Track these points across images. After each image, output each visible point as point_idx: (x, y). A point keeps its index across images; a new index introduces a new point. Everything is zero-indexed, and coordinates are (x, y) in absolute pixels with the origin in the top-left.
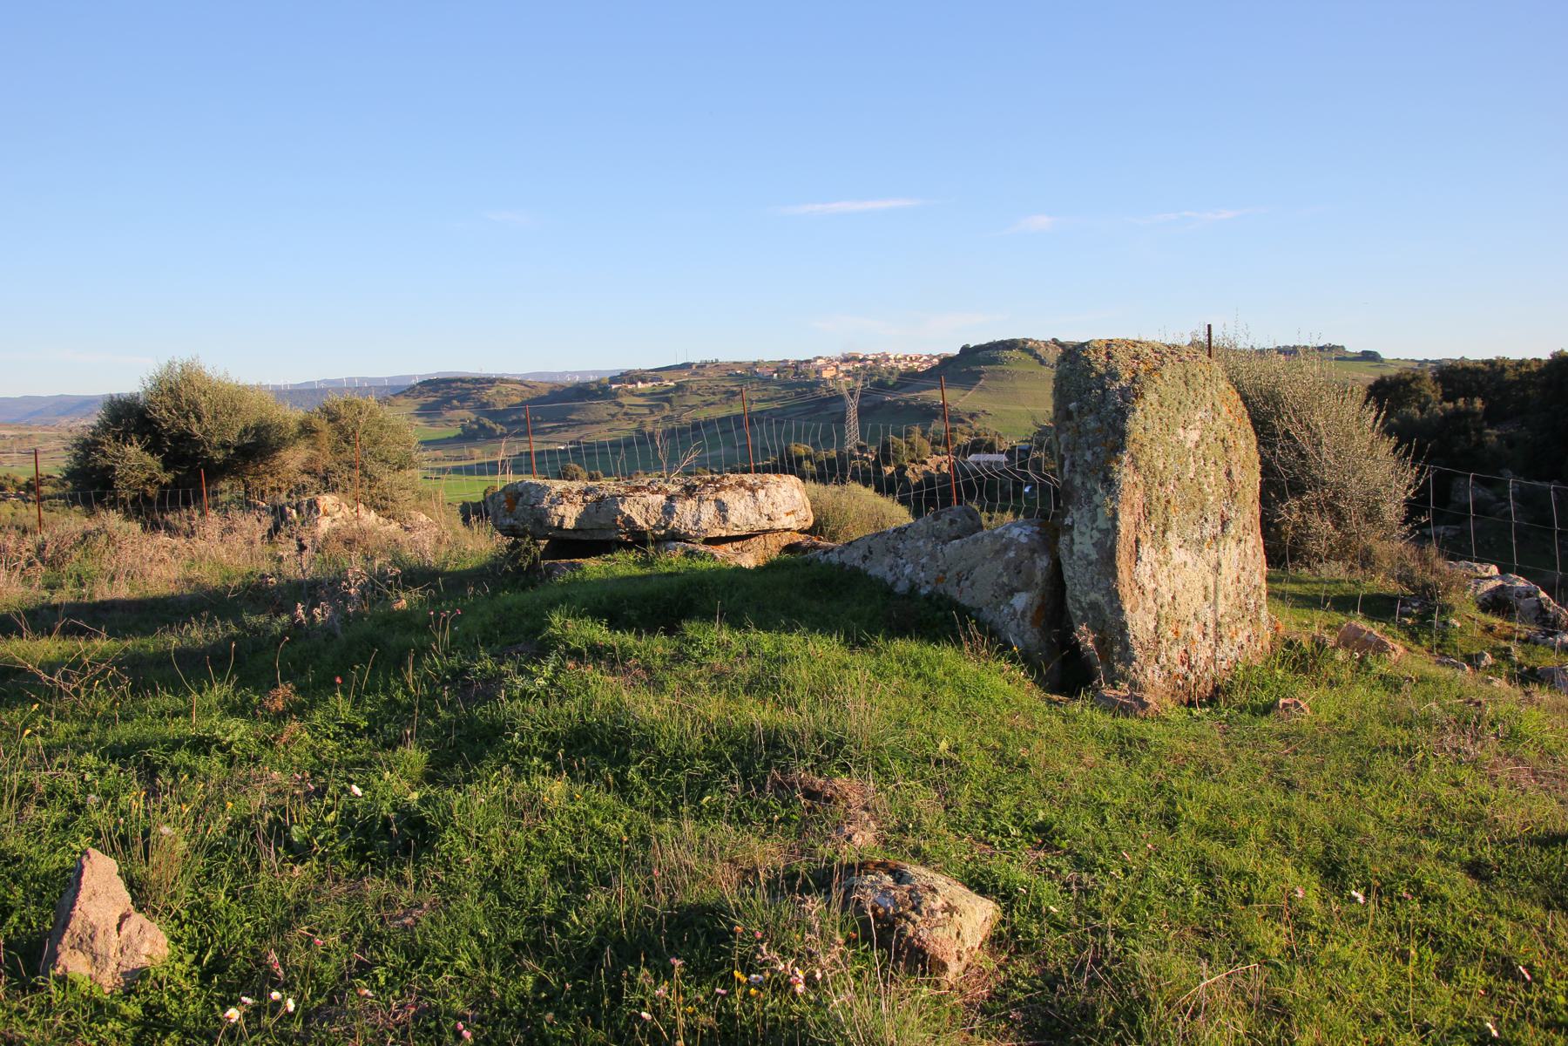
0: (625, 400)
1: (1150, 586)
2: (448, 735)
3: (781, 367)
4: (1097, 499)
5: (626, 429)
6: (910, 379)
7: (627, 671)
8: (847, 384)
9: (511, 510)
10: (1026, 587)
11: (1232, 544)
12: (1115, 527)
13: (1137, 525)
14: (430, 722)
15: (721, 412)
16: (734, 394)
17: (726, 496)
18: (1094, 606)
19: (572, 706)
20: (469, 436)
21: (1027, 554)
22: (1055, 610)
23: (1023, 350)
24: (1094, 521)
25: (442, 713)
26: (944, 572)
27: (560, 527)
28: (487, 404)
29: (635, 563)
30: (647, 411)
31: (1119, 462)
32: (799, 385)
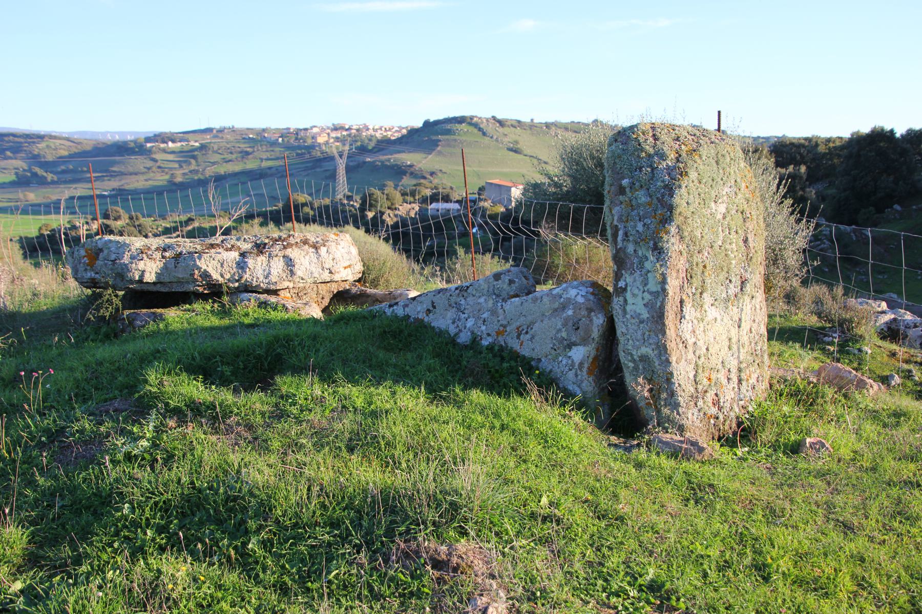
0: (158, 156)
1: (691, 341)
2: (50, 506)
3: (285, 133)
4: (648, 265)
5: (161, 179)
6: (385, 145)
7: (229, 430)
8: (337, 148)
9: (91, 265)
10: (584, 341)
11: (747, 299)
12: (664, 290)
13: (682, 288)
14: (28, 492)
15: (237, 167)
16: (248, 153)
17: (293, 253)
18: (644, 359)
19: (181, 472)
20: (23, 182)
21: (584, 313)
22: (608, 364)
23: (470, 124)
24: (646, 285)
25: (41, 480)
26: (505, 327)
27: (140, 281)
28: (38, 156)
29: (212, 312)
30: (177, 166)
31: (667, 232)
32: (299, 147)
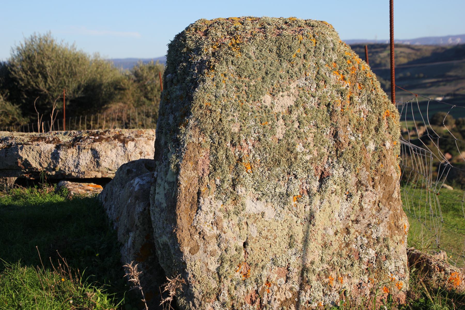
12: (177, 180)
13: (200, 180)
17: (100, 147)
31: (186, 125)
